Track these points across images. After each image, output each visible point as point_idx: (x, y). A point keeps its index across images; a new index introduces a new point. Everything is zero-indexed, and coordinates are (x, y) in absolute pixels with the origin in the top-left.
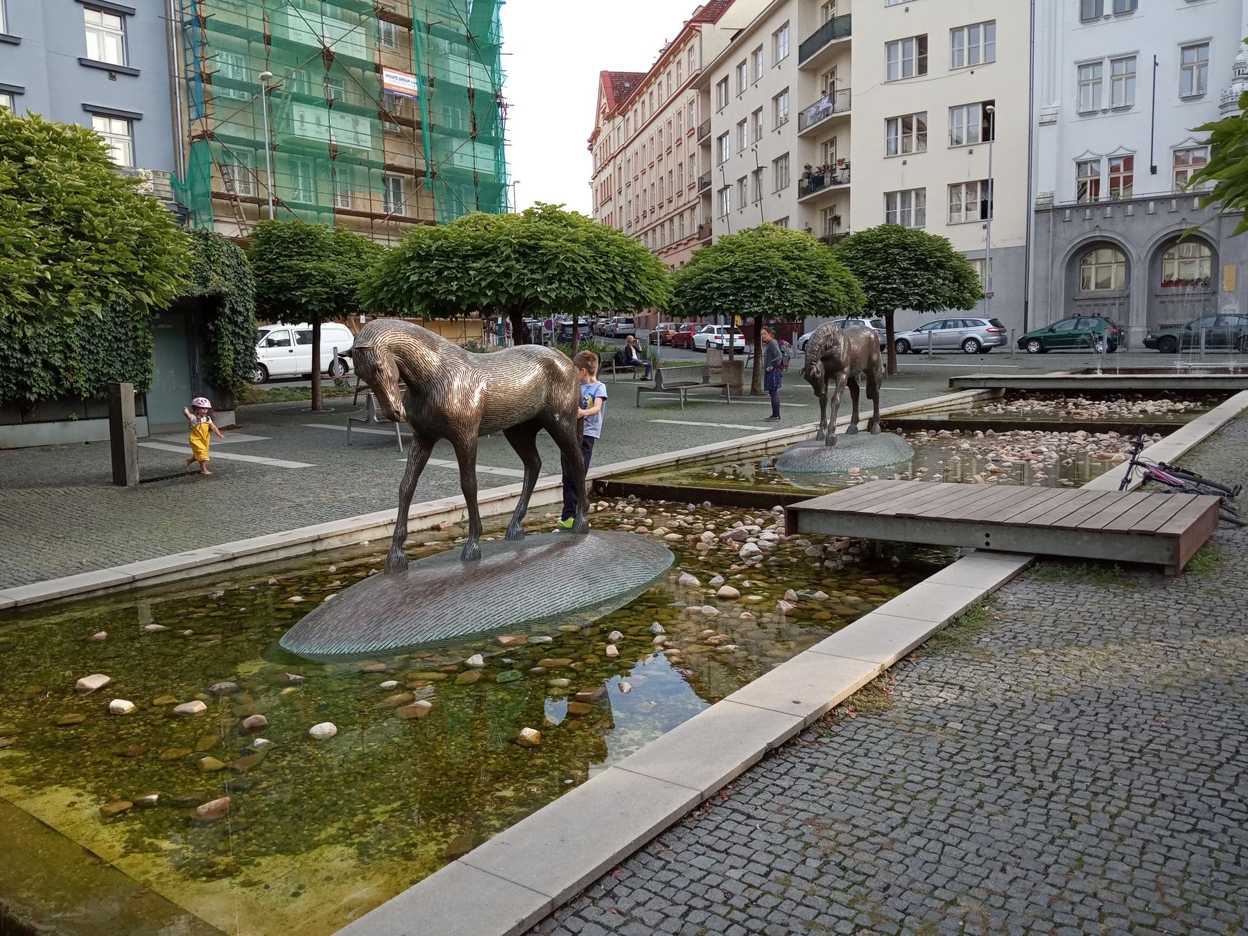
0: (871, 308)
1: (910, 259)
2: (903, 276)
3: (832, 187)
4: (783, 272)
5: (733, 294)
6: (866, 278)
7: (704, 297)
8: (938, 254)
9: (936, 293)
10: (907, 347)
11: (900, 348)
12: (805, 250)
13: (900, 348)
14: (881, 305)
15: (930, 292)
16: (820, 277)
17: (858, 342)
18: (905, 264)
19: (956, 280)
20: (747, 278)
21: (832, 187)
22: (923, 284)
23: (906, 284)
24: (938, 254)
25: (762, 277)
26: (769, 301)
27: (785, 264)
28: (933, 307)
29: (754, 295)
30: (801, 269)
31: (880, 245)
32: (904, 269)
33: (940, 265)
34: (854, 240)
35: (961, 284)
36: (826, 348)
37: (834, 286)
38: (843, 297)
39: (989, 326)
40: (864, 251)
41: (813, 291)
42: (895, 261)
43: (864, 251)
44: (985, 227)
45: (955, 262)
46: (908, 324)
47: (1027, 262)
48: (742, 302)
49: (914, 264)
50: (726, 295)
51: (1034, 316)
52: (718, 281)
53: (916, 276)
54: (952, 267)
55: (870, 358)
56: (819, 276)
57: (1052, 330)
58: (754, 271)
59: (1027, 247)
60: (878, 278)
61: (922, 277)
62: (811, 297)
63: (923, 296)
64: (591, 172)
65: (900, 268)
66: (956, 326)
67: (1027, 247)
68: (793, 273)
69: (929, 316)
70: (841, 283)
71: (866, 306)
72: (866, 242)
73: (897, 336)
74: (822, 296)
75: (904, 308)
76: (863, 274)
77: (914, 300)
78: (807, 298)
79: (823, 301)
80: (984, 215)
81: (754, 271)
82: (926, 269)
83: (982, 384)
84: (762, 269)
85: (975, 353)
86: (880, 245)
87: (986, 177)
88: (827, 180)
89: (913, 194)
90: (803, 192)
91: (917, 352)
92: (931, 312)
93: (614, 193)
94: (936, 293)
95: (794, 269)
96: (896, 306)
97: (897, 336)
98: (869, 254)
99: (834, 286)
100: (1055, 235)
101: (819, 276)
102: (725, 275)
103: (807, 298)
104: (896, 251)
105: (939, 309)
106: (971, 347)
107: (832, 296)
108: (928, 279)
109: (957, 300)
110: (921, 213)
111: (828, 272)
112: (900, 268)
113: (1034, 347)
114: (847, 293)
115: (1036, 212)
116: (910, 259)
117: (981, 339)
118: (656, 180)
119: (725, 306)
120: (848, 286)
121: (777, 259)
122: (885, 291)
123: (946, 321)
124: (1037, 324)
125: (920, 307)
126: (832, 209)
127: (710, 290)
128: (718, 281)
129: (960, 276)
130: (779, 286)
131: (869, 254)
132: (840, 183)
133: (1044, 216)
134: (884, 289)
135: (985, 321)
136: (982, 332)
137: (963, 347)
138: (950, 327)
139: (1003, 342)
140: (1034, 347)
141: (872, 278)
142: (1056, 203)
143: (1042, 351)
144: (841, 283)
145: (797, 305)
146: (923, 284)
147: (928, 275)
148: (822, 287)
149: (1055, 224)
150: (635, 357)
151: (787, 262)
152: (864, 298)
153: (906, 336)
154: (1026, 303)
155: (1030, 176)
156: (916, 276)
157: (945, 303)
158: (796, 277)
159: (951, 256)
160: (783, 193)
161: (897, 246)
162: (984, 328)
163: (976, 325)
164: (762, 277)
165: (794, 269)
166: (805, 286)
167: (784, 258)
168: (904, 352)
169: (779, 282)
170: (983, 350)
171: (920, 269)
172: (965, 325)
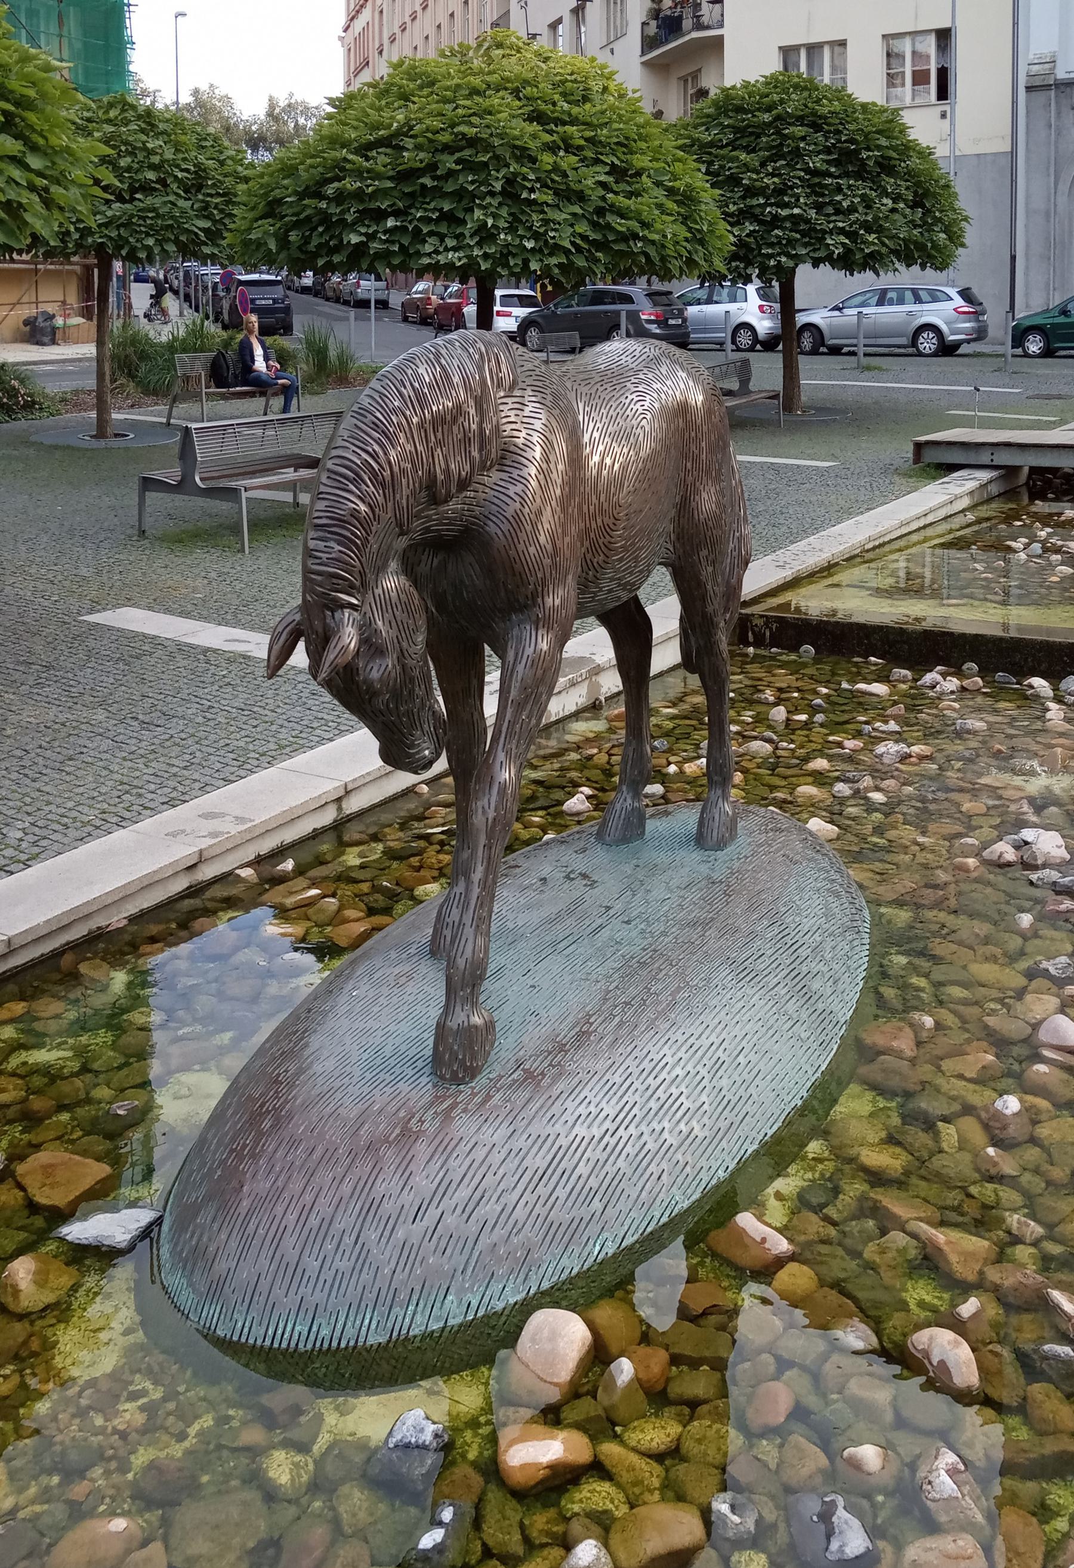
0: (749, 263)
1: (828, 151)
2: (815, 190)
3: (695, 35)
4: (524, 155)
5: (396, 214)
6: (739, 192)
7: (325, 218)
8: (883, 142)
9: (880, 230)
10: (822, 344)
11: (807, 342)
12: (586, 99)
13: (807, 342)
14: (764, 258)
15: (868, 228)
16: (618, 172)
17: (623, 435)
18: (816, 162)
19: (914, 205)
20: (432, 167)
21: (695, 35)
22: (852, 209)
23: (819, 207)
24: (883, 142)
25: (469, 166)
26: (485, 235)
27: (527, 132)
28: (872, 262)
29: (449, 218)
30: (569, 148)
31: (767, 117)
32: (815, 173)
33: (887, 167)
34: (715, 103)
35: (927, 212)
36: (433, 492)
37: (649, 201)
38: (672, 229)
39: (959, 301)
40: (736, 130)
41: (600, 212)
42: (797, 153)
43: (736, 130)
44: (943, 116)
45: (914, 162)
46: (824, 295)
47: (1013, 181)
48: (418, 237)
49: (836, 163)
50: (380, 216)
51: (1027, 285)
52: (359, 173)
53: (839, 189)
54: (910, 174)
55: (684, 506)
56: (614, 170)
57: (1065, 312)
58: (447, 149)
59: (1013, 153)
60: (761, 191)
61: (853, 193)
62: (595, 225)
63: (852, 235)
64: (342, 20)
65: (807, 170)
66: (901, 301)
67: (1013, 153)
68: (547, 159)
69: (865, 280)
70: (671, 192)
71: (734, 257)
72: (739, 109)
73: (801, 319)
74: (620, 224)
75: (816, 265)
76: (734, 181)
77: (836, 244)
78: (582, 228)
79: (624, 238)
80: (943, 93)
81: (447, 149)
82: (858, 176)
83: (985, 458)
84: (473, 142)
85: (935, 355)
86: (767, 117)
87: (946, 24)
88: (687, 24)
89: (827, 51)
90: (649, 43)
91: (835, 351)
92: (869, 274)
93: (373, 55)
94: (880, 230)
95: (552, 148)
96: (798, 259)
97: (801, 319)
98: (746, 136)
99: (649, 201)
100: (1059, 134)
101: (614, 170)
102: (381, 159)
103: (582, 228)
104: (799, 131)
105: (884, 266)
106: (928, 343)
107: (645, 225)
108: (863, 197)
109: (921, 247)
110: (839, 68)
111: (641, 161)
112: (807, 170)
113: (1034, 346)
114: (685, 220)
115: (1029, 89)
116: (828, 151)
117: (944, 328)
118: (431, 31)
119: (375, 246)
120: (687, 199)
121: (509, 119)
122: (776, 222)
123: (884, 292)
124: (1032, 303)
125: (847, 263)
126: (695, 75)
127: (340, 198)
128: (359, 173)
129: (927, 194)
130: (511, 192)
131: (746, 136)
132: (708, 28)
133: (1040, 97)
134: (775, 217)
135: (952, 292)
136: (945, 313)
137: (914, 343)
138: (891, 303)
139: (980, 334)
140: (1034, 346)
141: (750, 192)
142: (1061, 74)
143: (1048, 353)
144: (671, 192)
145: (556, 249)
146: (852, 209)
147: (863, 188)
148: (621, 201)
149: (1059, 113)
150: (260, 364)
151: (535, 127)
152: (727, 237)
153: (817, 318)
154: (1013, 258)
155: (1015, 24)
156: (839, 189)
157: (896, 253)
158: (556, 168)
159: (908, 148)
160: (616, 46)
161: (800, 120)
162: (949, 306)
163: (935, 300)
164: (469, 166)
165: (552, 148)
166: (581, 197)
167: (530, 119)
168: (814, 352)
169: (510, 181)
170: (947, 349)
171: (847, 175)
172: (918, 300)
